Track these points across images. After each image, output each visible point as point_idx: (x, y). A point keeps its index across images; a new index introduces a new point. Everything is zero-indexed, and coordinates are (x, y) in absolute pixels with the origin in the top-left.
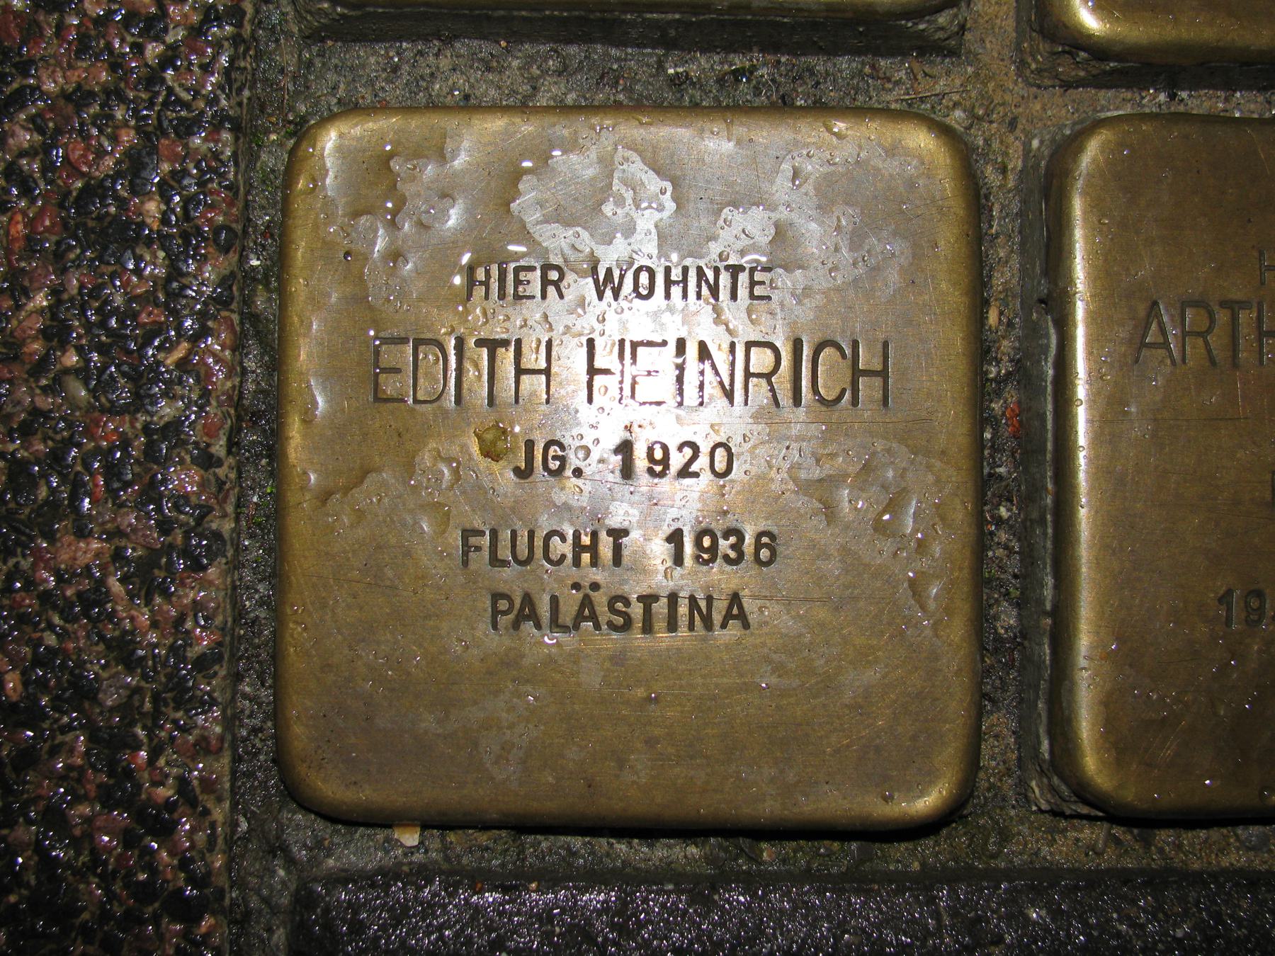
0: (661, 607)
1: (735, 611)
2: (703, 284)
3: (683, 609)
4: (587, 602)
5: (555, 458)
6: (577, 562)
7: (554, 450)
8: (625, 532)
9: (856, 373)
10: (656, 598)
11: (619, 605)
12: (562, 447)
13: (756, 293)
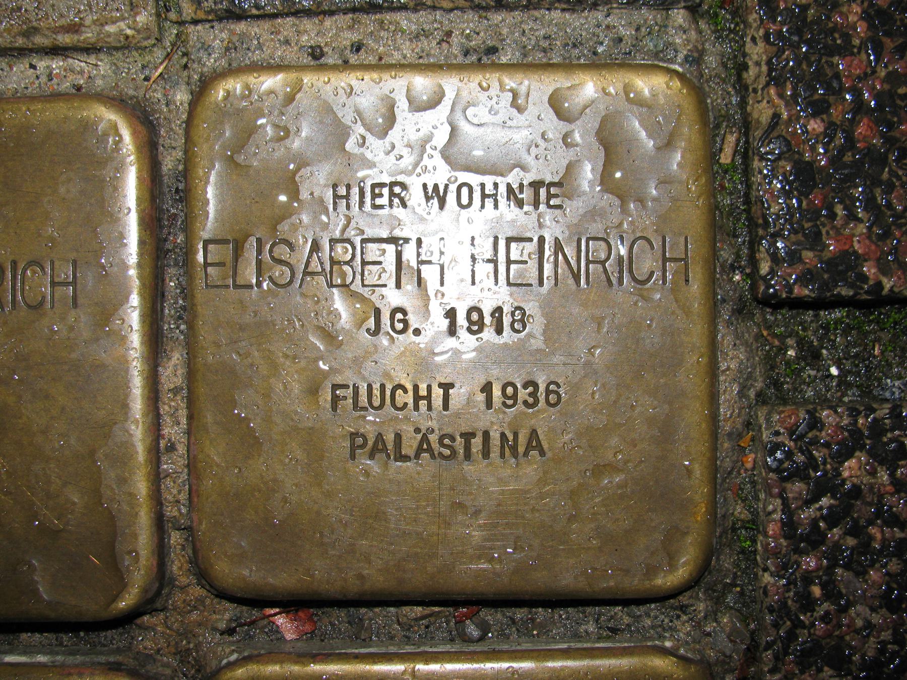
0: (477, 443)
1: (425, 446)
4: (425, 438)
6: (416, 407)
7: (399, 316)
8: (452, 386)
9: (665, 260)
10: (473, 435)
11: (447, 441)
13: (552, 203)
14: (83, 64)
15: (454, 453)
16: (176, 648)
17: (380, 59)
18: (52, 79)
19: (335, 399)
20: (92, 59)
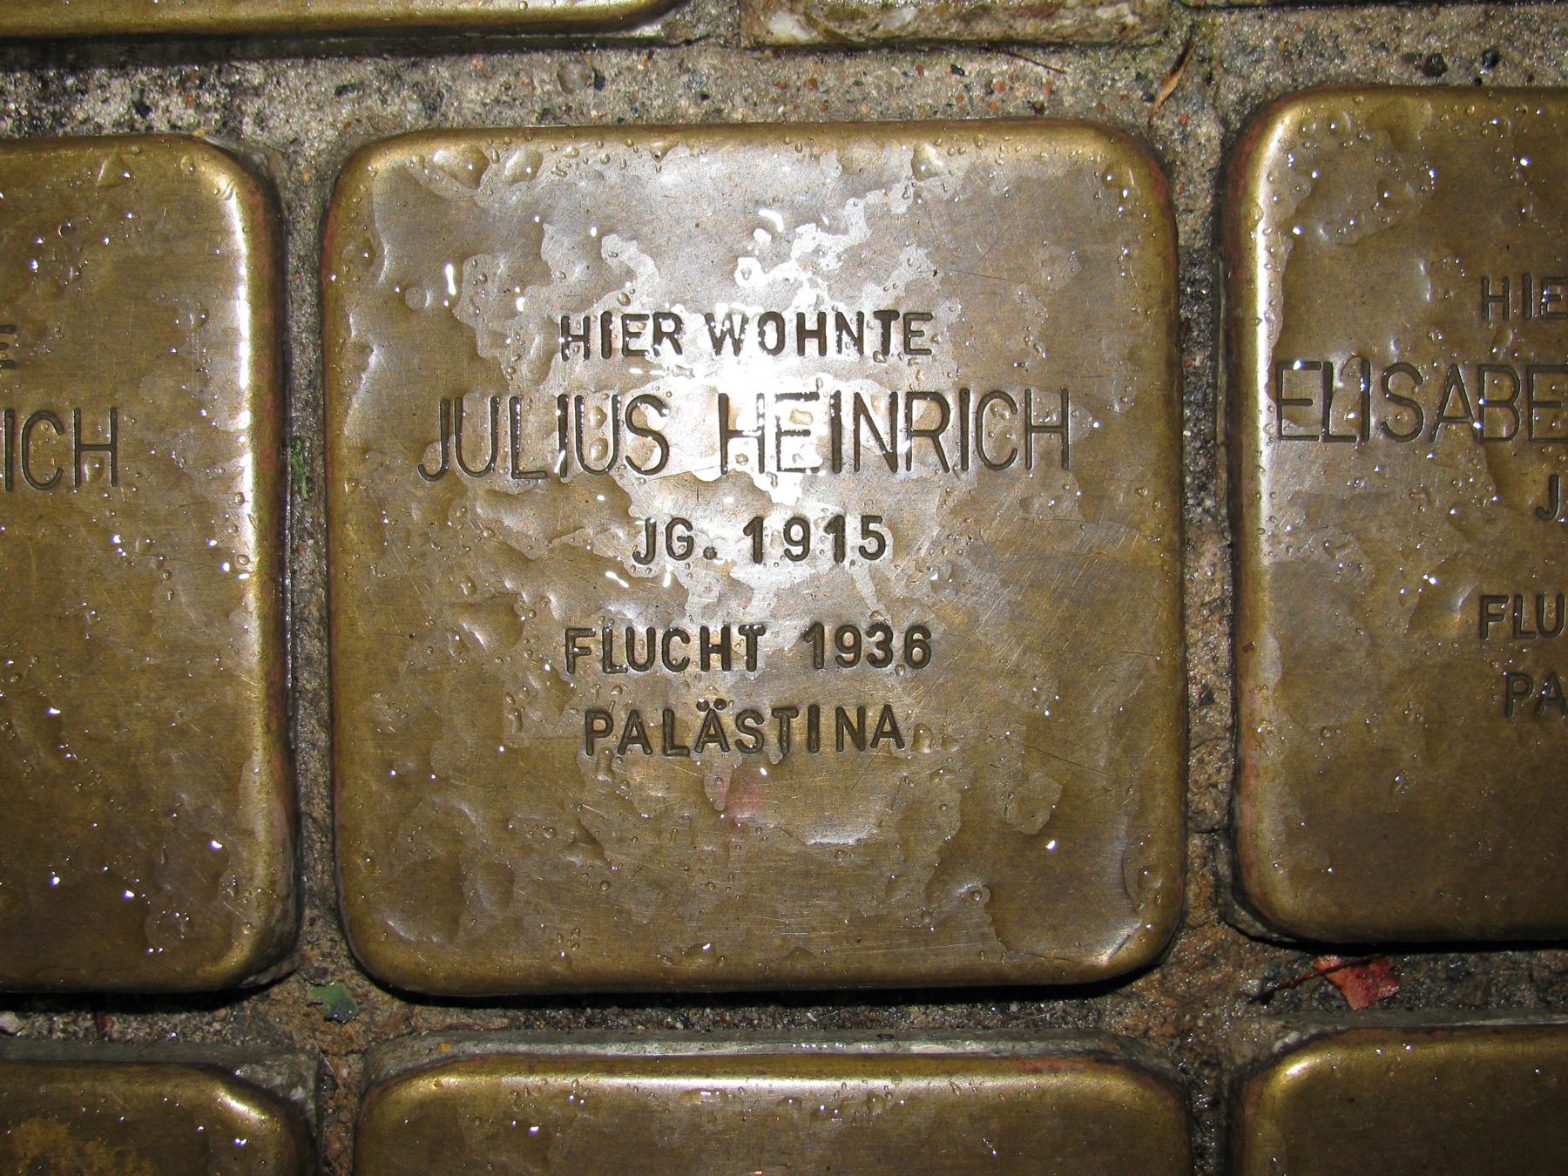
1: (887, 727)
3: (827, 721)
4: (712, 720)
5: (680, 539)
6: (705, 665)
7: (679, 530)
9: (1029, 428)
10: (793, 710)
11: (750, 722)
12: (689, 526)
14: (1040, 69)
16: (1176, 1028)
17: (1531, 78)
18: (992, 92)
20: (1055, 63)
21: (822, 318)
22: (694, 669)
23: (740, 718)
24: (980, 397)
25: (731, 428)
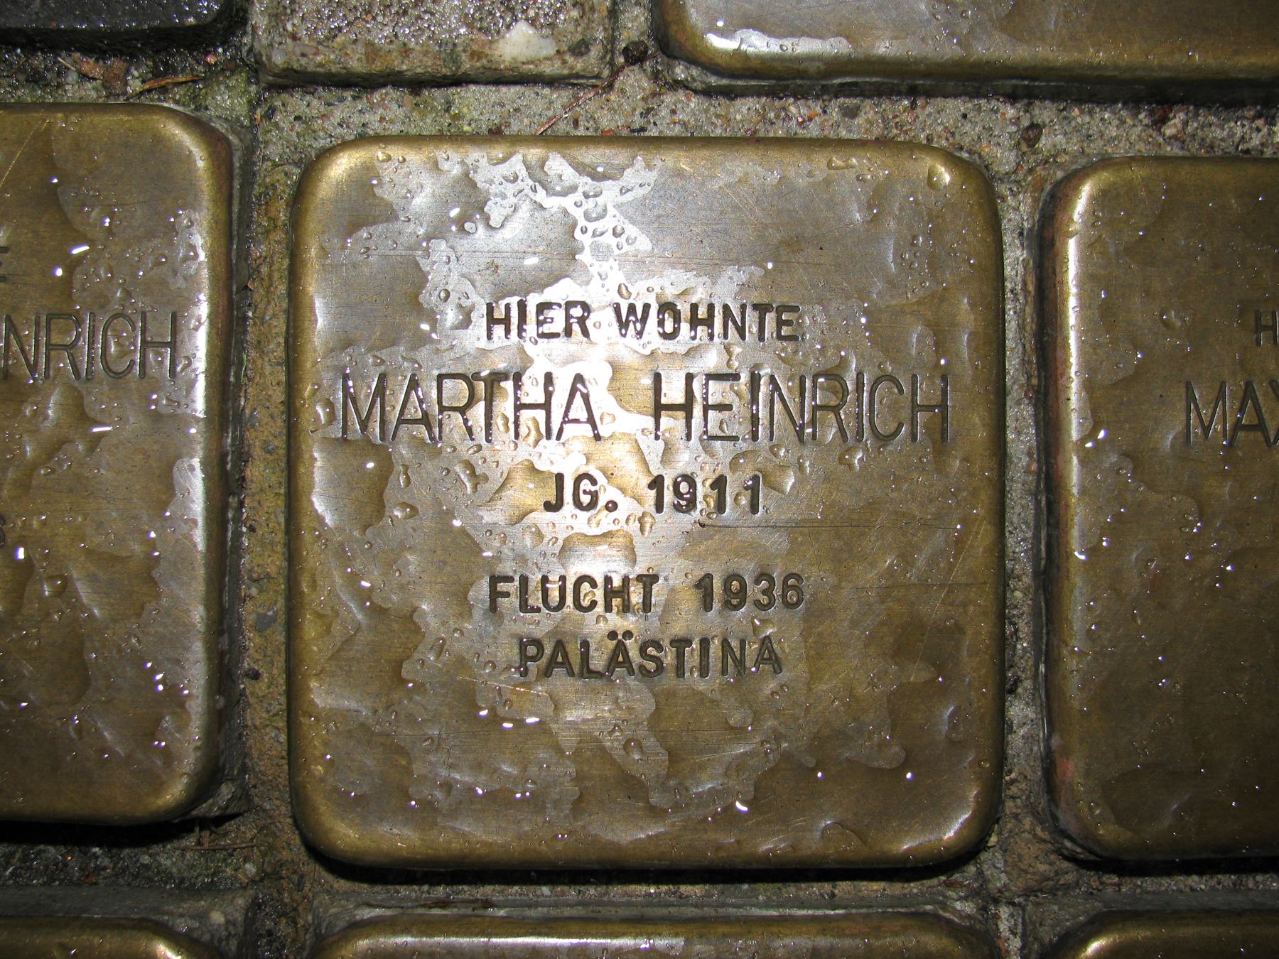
0: (692, 656)
1: (560, 659)
2: (730, 323)
3: (715, 647)
7: (585, 485)
8: (654, 578)
9: (915, 407)
10: (688, 642)
11: (651, 651)
12: (594, 482)
15: (660, 668)
19: (495, 595)
21: (711, 307)
22: (600, 609)
23: (643, 650)
24: (873, 379)
25: (663, 412)
